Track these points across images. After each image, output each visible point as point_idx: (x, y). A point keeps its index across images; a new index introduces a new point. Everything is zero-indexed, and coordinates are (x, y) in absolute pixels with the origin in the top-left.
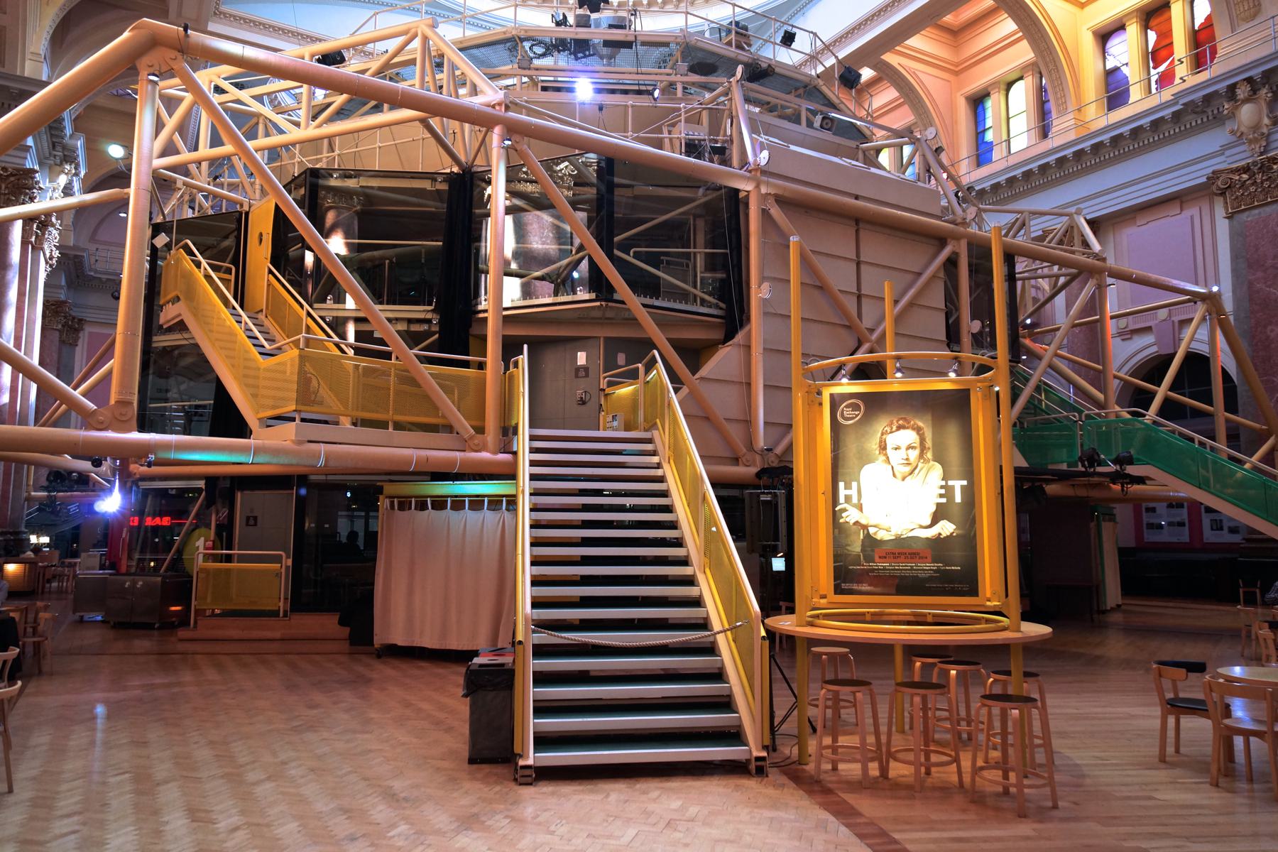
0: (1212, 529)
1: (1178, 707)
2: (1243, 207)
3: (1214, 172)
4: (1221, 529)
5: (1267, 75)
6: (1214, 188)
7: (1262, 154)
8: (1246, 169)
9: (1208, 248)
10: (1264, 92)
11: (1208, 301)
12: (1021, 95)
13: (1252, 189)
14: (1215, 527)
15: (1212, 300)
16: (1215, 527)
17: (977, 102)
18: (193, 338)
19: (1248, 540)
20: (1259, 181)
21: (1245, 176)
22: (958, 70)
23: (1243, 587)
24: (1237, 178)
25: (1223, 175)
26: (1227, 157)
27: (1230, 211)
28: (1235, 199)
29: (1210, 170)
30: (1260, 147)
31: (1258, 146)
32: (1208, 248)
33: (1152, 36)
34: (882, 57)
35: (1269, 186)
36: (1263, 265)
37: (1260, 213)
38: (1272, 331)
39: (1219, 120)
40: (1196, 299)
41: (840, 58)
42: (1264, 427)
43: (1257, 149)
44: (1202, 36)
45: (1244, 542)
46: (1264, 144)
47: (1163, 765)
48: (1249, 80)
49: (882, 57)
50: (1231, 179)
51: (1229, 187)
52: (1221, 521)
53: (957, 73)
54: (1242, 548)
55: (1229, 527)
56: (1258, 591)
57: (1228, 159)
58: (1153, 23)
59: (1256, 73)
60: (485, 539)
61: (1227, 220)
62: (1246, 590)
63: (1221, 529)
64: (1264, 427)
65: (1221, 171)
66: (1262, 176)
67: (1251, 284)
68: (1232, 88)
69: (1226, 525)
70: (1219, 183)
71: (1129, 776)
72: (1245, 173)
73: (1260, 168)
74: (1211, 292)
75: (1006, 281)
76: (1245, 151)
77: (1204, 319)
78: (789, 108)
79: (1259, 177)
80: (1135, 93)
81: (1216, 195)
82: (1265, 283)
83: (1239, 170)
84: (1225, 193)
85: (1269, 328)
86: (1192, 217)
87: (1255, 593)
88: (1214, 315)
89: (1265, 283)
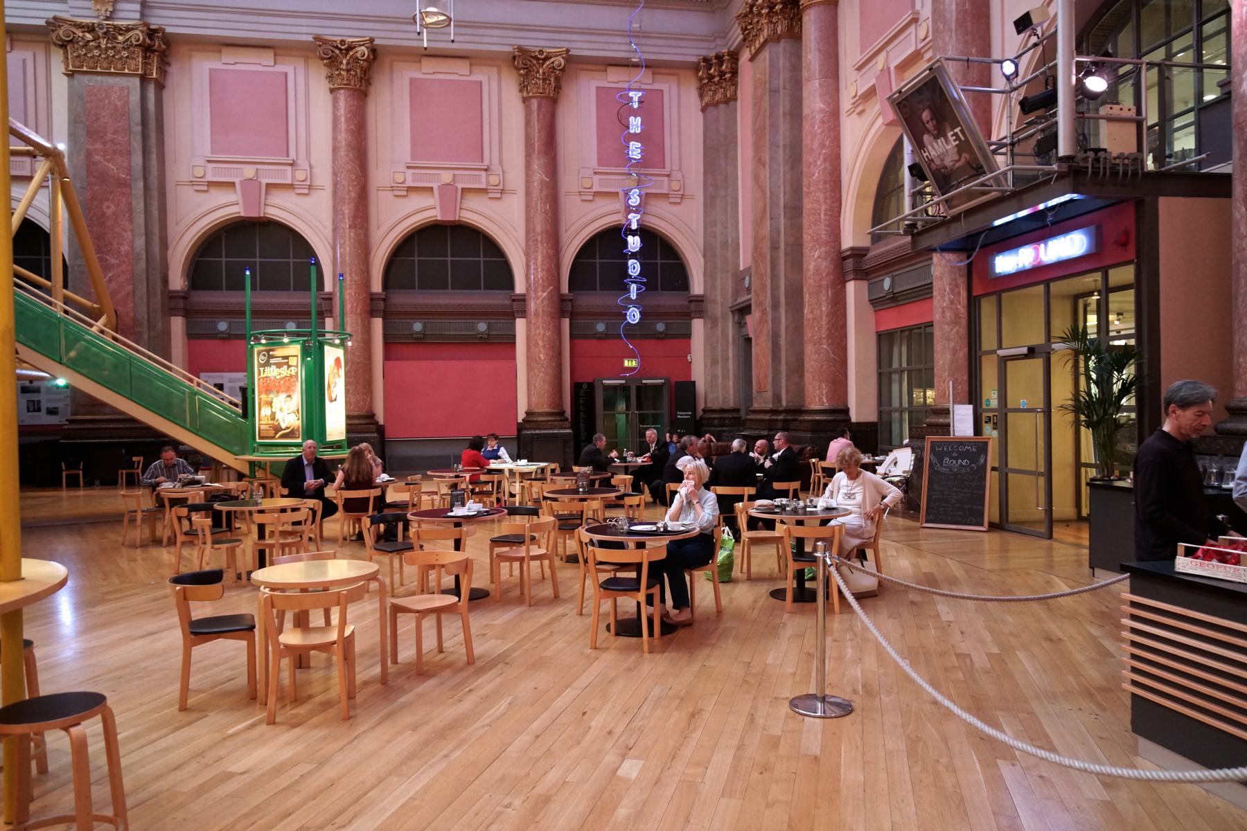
0: (28, 411)
1: (201, 631)
2: (85, 69)
3: (55, 18)
4: (39, 410)
6: (54, 36)
7: (107, 18)
8: (91, 29)
9: (42, 103)
11: (50, 158)
13: (96, 52)
14: (32, 409)
15: (52, 155)
16: (32, 409)
19: (71, 422)
20: (103, 46)
21: (89, 36)
23: (66, 470)
24: (81, 34)
25: (66, 26)
26: (70, 7)
27: (71, 68)
28: (77, 57)
29: (50, 15)
30: (106, 11)
31: (104, 9)
32: (42, 103)
35: (113, 56)
36: (102, 137)
37: (102, 81)
38: (108, 207)
40: (37, 152)
42: (95, 305)
43: (103, 12)
45: (67, 423)
46: (111, 9)
47: (185, 717)
50: (74, 33)
51: (71, 41)
52: (39, 402)
54: (65, 429)
55: (47, 408)
56: (81, 472)
57: (70, 10)
60: (552, 411)
61: (66, 78)
62: (68, 472)
63: (39, 410)
64: (95, 305)
65: (65, 21)
66: (107, 43)
67: (89, 154)
69: (44, 407)
70: (61, 33)
71: (167, 750)
72: (89, 32)
73: (105, 33)
74: (56, 148)
76: (90, 9)
77: (45, 179)
79: (103, 42)
81: (55, 44)
82: (104, 156)
83: (83, 27)
84: (66, 47)
85: (106, 204)
86: (24, 61)
87: (79, 474)
88: (57, 176)
89: (104, 156)
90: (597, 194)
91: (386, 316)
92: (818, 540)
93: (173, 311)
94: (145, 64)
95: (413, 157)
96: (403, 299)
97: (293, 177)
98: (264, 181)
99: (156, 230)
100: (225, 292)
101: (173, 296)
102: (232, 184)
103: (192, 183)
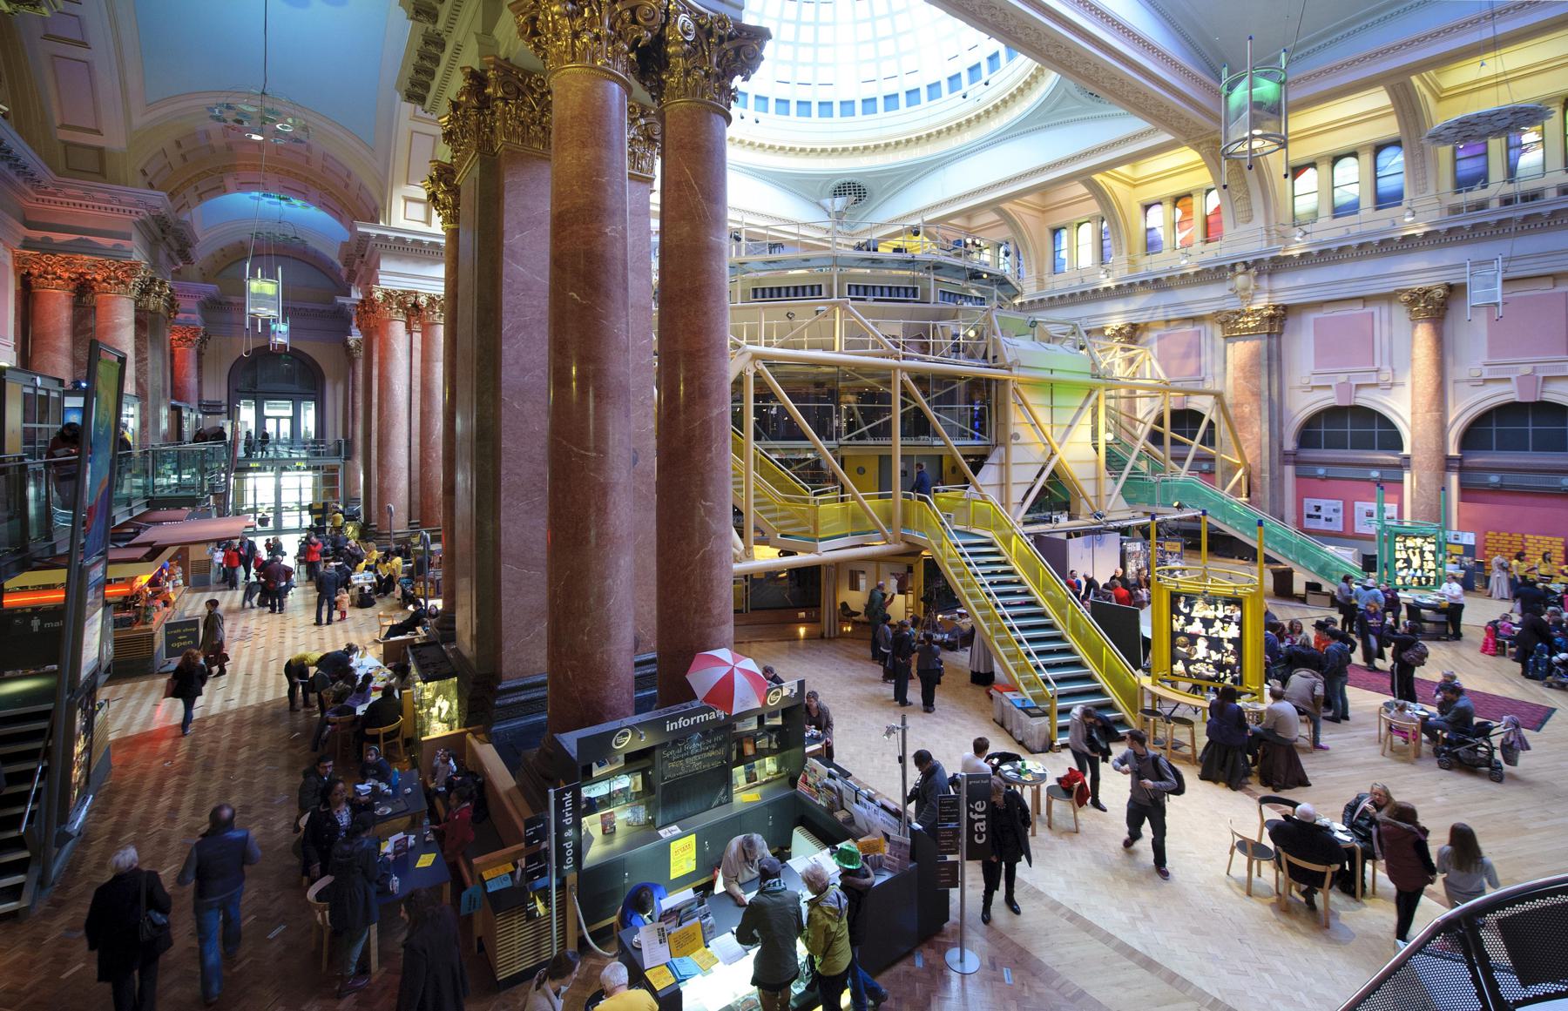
5: (1256, 262)
10: (1252, 271)
12: (1087, 233)
17: (1056, 231)
18: (84, 44)
22: (1044, 211)
33: (1179, 212)
34: (418, 866)
39: (1222, 280)
41: (490, 890)
44: (1211, 220)
48: (1245, 263)
49: (418, 866)
53: (1043, 212)
58: (1179, 204)
59: (1250, 260)
68: (1234, 265)
75: (389, 489)
78: (547, 905)
80: (1166, 252)
90: (1313, 387)
91: (1462, 470)
92: (1240, 624)
93: (1287, 463)
94: (1271, 326)
95: (1316, 367)
96: (1478, 459)
97: (1378, 379)
98: (1354, 383)
99: (1276, 418)
100: (1349, 451)
101: (1286, 454)
102: (1330, 387)
103: (1301, 387)
